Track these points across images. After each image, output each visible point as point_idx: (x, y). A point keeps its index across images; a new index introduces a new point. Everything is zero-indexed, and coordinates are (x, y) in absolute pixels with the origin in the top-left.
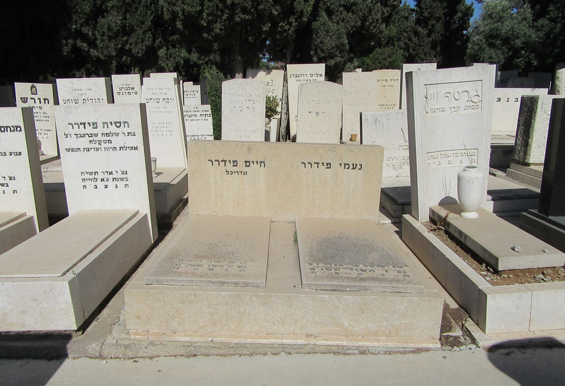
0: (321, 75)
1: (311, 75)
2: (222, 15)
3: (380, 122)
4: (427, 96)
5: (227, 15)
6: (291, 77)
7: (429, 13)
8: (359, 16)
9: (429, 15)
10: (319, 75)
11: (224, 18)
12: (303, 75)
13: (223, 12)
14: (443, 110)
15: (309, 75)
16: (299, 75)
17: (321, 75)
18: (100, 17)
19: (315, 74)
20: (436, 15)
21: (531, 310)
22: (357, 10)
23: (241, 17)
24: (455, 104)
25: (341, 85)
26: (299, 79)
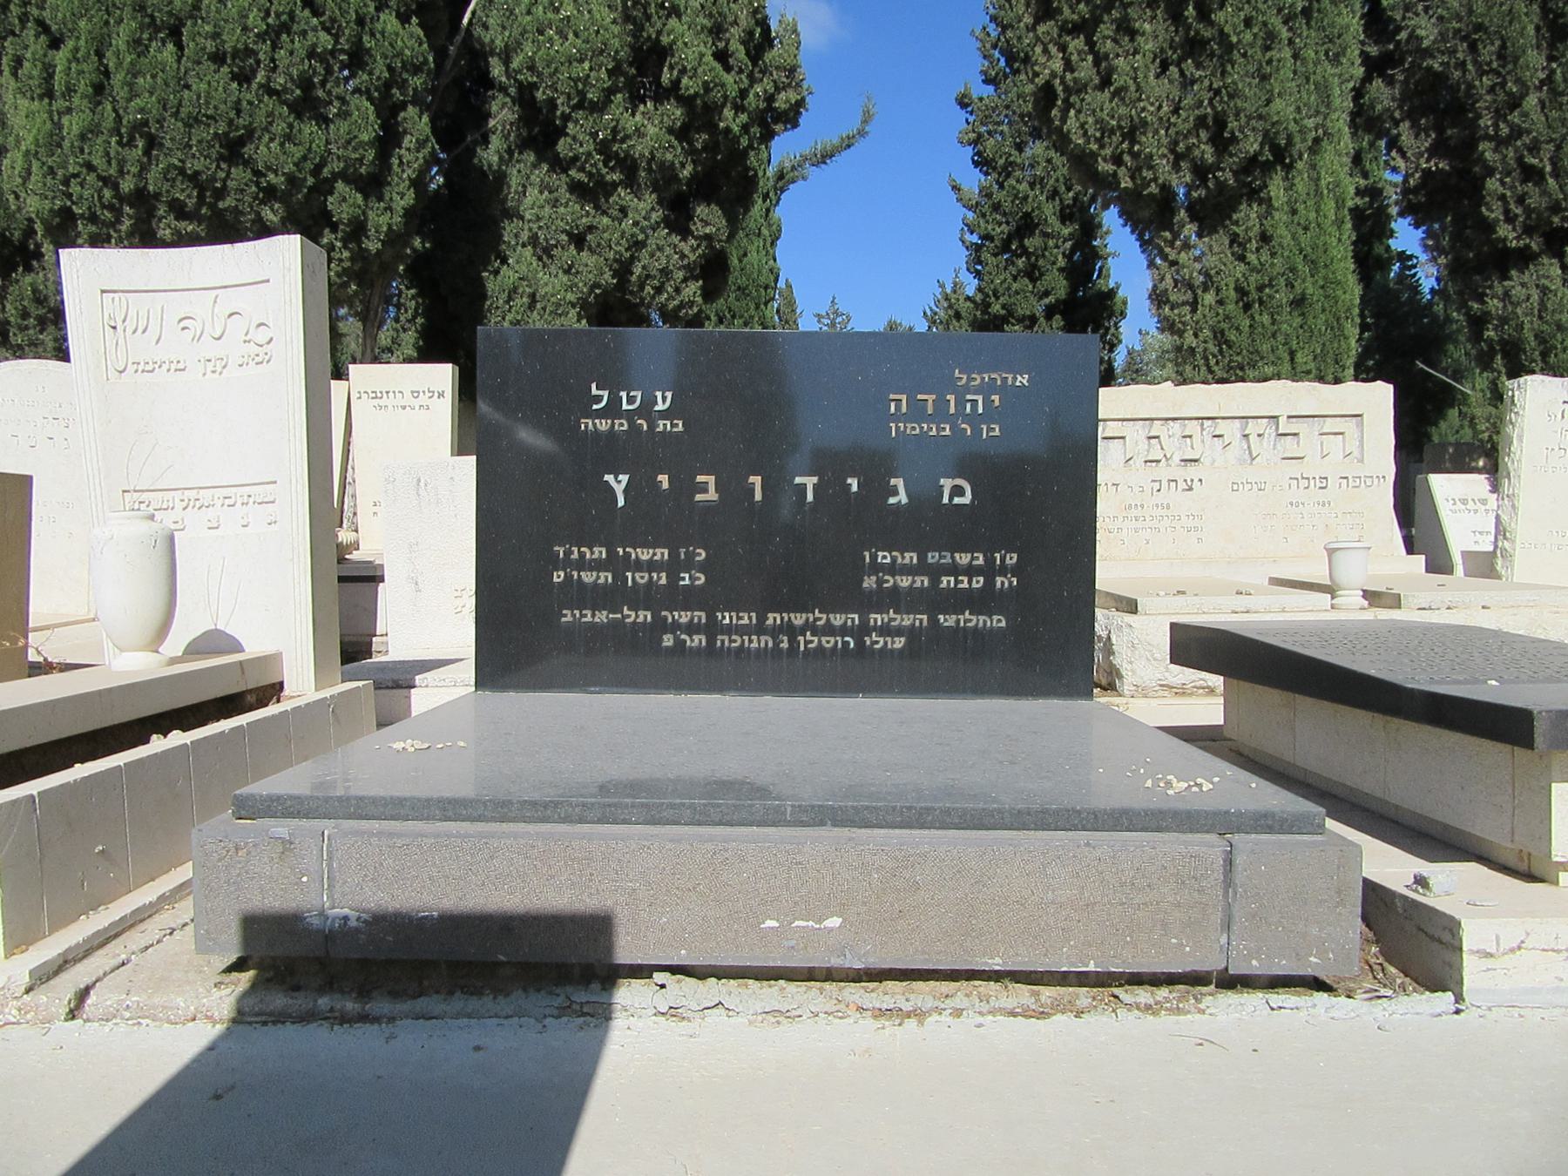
0: (441, 395)
1: (416, 395)
2: (118, 221)
3: (429, 487)
4: (113, 324)
6: (360, 398)
7: (1003, 307)
8: (606, 260)
9: (1004, 312)
10: (436, 394)
11: (123, 228)
12: (394, 392)
13: (118, 213)
14: (181, 366)
15: (407, 394)
17: (441, 395)
18: (21, 269)
19: (424, 392)
22: (599, 245)
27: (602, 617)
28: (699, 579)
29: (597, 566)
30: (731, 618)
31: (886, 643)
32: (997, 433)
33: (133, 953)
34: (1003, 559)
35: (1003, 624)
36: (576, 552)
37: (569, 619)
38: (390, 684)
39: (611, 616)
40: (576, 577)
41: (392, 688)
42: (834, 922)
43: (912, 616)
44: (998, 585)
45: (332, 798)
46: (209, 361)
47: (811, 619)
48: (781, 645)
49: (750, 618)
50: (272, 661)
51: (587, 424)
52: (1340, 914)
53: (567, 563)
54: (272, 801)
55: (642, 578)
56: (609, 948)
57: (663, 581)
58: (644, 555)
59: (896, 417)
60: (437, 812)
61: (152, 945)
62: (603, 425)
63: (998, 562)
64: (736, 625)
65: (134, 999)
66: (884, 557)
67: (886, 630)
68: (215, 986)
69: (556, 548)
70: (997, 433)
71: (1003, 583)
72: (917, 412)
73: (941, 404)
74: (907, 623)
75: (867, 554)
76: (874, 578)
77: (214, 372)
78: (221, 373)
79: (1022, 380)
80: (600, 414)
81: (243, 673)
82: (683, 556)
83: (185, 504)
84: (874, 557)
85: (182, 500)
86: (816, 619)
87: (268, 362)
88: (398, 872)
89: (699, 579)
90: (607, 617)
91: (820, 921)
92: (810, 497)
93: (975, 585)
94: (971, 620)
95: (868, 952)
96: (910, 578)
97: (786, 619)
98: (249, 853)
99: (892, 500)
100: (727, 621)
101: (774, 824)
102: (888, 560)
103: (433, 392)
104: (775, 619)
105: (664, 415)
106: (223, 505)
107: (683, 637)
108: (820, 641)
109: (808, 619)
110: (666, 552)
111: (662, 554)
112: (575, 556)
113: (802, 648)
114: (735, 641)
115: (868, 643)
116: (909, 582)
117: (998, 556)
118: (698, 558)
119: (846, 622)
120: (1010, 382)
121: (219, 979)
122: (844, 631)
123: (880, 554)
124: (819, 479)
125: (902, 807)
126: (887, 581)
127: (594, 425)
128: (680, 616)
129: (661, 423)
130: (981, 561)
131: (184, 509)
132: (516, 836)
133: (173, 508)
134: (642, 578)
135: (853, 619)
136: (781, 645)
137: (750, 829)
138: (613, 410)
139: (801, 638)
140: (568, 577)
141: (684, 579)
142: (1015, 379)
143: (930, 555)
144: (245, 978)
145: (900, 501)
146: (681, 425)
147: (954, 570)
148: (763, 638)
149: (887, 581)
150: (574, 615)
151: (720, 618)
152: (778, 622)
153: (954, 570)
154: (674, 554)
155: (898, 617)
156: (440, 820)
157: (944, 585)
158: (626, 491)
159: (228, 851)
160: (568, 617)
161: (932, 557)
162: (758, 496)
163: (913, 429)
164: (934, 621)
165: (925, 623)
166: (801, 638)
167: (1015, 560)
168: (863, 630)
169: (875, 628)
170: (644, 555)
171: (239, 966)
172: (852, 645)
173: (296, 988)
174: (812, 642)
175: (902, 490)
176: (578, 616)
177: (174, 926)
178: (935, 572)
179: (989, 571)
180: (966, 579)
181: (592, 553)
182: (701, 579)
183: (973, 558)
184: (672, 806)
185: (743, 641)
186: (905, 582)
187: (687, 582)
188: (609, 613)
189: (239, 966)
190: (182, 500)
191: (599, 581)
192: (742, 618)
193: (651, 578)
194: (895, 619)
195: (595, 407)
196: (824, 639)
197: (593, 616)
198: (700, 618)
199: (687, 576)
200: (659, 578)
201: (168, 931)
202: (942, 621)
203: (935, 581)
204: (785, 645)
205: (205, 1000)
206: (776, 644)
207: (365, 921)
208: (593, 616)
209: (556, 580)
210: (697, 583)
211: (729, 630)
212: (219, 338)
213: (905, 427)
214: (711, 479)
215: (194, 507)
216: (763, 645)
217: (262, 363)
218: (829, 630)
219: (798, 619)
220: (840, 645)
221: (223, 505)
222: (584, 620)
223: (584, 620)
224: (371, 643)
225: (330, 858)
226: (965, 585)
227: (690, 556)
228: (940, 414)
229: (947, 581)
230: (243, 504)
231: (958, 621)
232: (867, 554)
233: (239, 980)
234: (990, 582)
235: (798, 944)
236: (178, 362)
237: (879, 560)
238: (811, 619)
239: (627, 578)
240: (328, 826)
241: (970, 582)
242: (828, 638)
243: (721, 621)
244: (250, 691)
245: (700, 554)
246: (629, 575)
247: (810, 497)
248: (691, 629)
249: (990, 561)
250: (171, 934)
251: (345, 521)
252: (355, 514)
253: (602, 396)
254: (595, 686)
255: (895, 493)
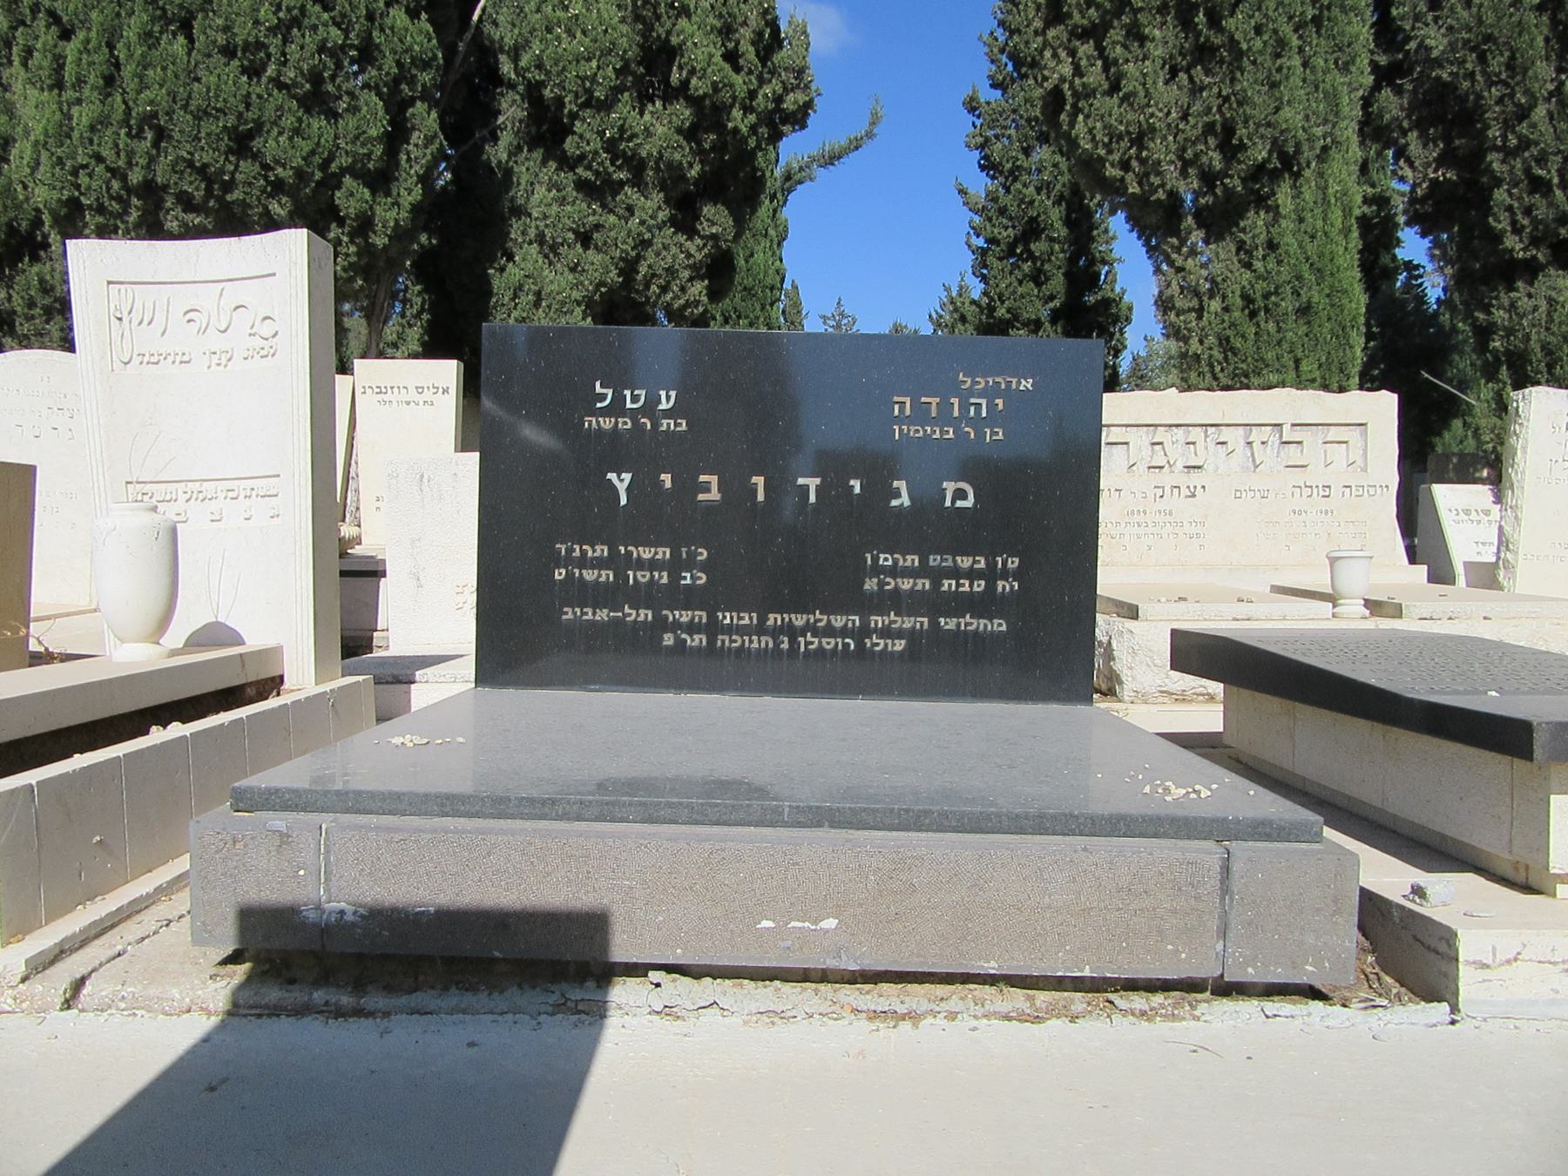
0: (445, 391)
1: (420, 390)
2: (126, 212)
3: (432, 482)
4: (119, 316)
5: (139, 213)
6: (364, 393)
7: (1008, 311)
10: (441, 390)
11: (131, 219)
13: (126, 205)
14: (186, 358)
15: (412, 390)
16: (386, 387)
17: (445, 391)
18: (27, 259)
20: (1025, 315)
21: (108, 961)
22: (605, 243)
23: (180, 219)
24: (215, 341)
25: (229, 950)
26: (385, 397)
27: (603, 615)
28: (700, 578)
29: (599, 564)
30: (732, 618)
31: (886, 645)
32: (1000, 436)
33: (129, 944)
34: (1005, 563)
35: (1004, 628)
36: (578, 550)
37: (570, 616)
38: (390, 679)
39: (611, 614)
40: (577, 575)
41: (392, 683)
42: (830, 923)
43: (912, 619)
44: (1000, 589)
45: (329, 791)
46: (215, 353)
47: (812, 621)
48: (782, 646)
49: (751, 618)
50: (273, 654)
51: (590, 422)
52: (1336, 923)
53: (568, 561)
54: (271, 794)
55: (644, 577)
56: (605, 945)
57: (665, 580)
58: (647, 553)
59: (900, 420)
60: (435, 808)
61: (148, 936)
62: (607, 423)
63: (1000, 565)
64: (737, 625)
65: (129, 990)
66: (886, 560)
67: (886, 633)
68: (211, 978)
69: (558, 546)
70: (1000, 436)
71: (1004, 587)
72: (920, 415)
73: (945, 407)
74: (907, 625)
75: (869, 556)
76: (875, 580)
77: (219, 365)
78: (226, 366)
79: (1027, 384)
80: (605, 412)
81: (243, 666)
82: (684, 556)
83: (188, 496)
84: (875, 559)
85: (185, 493)
86: (817, 621)
87: (273, 355)
88: (395, 866)
89: (700, 578)
90: (608, 616)
91: (816, 922)
92: (812, 498)
93: (976, 589)
94: (972, 624)
95: (863, 954)
96: (911, 581)
97: (787, 620)
98: (246, 845)
99: (894, 503)
100: (728, 621)
101: (772, 825)
102: (890, 563)
103: (438, 388)
104: (776, 619)
105: (668, 414)
106: (225, 498)
107: (684, 636)
108: (820, 643)
109: (808, 620)
110: (668, 551)
111: (664, 553)
112: (577, 553)
113: (802, 649)
114: (735, 641)
115: (869, 645)
116: (911, 584)
117: (999, 560)
118: (699, 558)
119: (846, 624)
120: (1014, 386)
121: (214, 971)
122: (844, 632)
123: (882, 556)
124: (822, 482)
125: (900, 810)
126: (889, 584)
127: (598, 422)
128: (681, 616)
129: (665, 422)
130: (982, 565)
131: (187, 501)
132: (513, 833)
133: (176, 500)
134: (644, 577)
135: (854, 621)
136: (782, 646)
137: (747, 829)
138: (617, 408)
139: (801, 639)
140: (570, 575)
141: (685, 578)
142: (1019, 383)
143: (931, 557)
144: (241, 971)
145: (902, 504)
146: (684, 424)
147: (956, 573)
148: (763, 639)
149: (889, 584)
150: (575, 613)
151: (721, 617)
152: (779, 623)
153: (956, 573)
154: (675, 553)
155: (899, 619)
156: (438, 815)
157: (945, 588)
158: (628, 490)
159: (226, 844)
160: (569, 614)
161: (934, 560)
162: (761, 497)
163: (916, 431)
164: (934, 624)
165: (926, 626)
166: (801, 639)
167: (1016, 564)
168: (864, 632)
169: (875, 630)
170: (647, 553)
171: (234, 959)
172: (852, 647)
173: (292, 982)
174: (812, 643)
175: (904, 493)
176: (579, 614)
177: (171, 917)
178: (937, 575)
179: (991, 575)
180: (967, 583)
181: (594, 551)
182: (703, 579)
183: (975, 562)
184: (670, 805)
185: (743, 641)
186: (906, 584)
187: (688, 581)
188: (610, 611)
189: (234, 959)
190: (185, 493)
191: (601, 580)
192: (743, 618)
193: (652, 577)
194: (895, 622)
195: (599, 405)
196: (824, 641)
197: (594, 614)
198: (701, 617)
199: (688, 575)
200: (661, 577)
201: (165, 923)
202: (942, 624)
203: (936, 584)
204: (785, 646)
205: (200, 992)
206: (777, 645)
207: (362, 916)
208: (594, 614)
209: (557, 577)
210: (698, 582)
211: (730, 630)
212: (224, 331)
213: (909, 430)
214: (714, 480)
215: (197, 499)
216: (763, 645)
217: (267, 356)
218: (830, 631)
219: (799, 621)
220: (840, 647)
221: (225, 498)
222: (585, 617)
223: (585, 617)
224: (371, 638)
225: (327, 852)
226: (966, 588)
227: (692, 556)
228: (944, 418)
229: (948, 584)
230: (246, 497)
231: (959, 624)
232: (869, 556)
233: (234, 972)
234: (991, 586)
235: (793, 945)
236: (184, 354)
237: (881, 563)
238: (812, 621)
239: (629, 576)
240: (326, 820)
241: (971, 586)
242: (829, 640)
243: (722, 621)
244: (250, 684)
245: (701, 554)
246: (631, 573)
247: (812, 498)
248: (692, 628)
249: (991, 565)
250: (167, 925)
251: (348, 515)
252: (358, 509)
253: (606, 395)
254: (595, 684)
255: (898, 495)
